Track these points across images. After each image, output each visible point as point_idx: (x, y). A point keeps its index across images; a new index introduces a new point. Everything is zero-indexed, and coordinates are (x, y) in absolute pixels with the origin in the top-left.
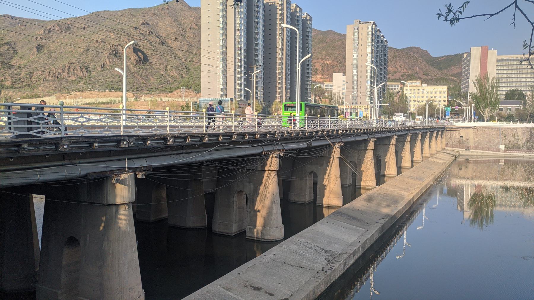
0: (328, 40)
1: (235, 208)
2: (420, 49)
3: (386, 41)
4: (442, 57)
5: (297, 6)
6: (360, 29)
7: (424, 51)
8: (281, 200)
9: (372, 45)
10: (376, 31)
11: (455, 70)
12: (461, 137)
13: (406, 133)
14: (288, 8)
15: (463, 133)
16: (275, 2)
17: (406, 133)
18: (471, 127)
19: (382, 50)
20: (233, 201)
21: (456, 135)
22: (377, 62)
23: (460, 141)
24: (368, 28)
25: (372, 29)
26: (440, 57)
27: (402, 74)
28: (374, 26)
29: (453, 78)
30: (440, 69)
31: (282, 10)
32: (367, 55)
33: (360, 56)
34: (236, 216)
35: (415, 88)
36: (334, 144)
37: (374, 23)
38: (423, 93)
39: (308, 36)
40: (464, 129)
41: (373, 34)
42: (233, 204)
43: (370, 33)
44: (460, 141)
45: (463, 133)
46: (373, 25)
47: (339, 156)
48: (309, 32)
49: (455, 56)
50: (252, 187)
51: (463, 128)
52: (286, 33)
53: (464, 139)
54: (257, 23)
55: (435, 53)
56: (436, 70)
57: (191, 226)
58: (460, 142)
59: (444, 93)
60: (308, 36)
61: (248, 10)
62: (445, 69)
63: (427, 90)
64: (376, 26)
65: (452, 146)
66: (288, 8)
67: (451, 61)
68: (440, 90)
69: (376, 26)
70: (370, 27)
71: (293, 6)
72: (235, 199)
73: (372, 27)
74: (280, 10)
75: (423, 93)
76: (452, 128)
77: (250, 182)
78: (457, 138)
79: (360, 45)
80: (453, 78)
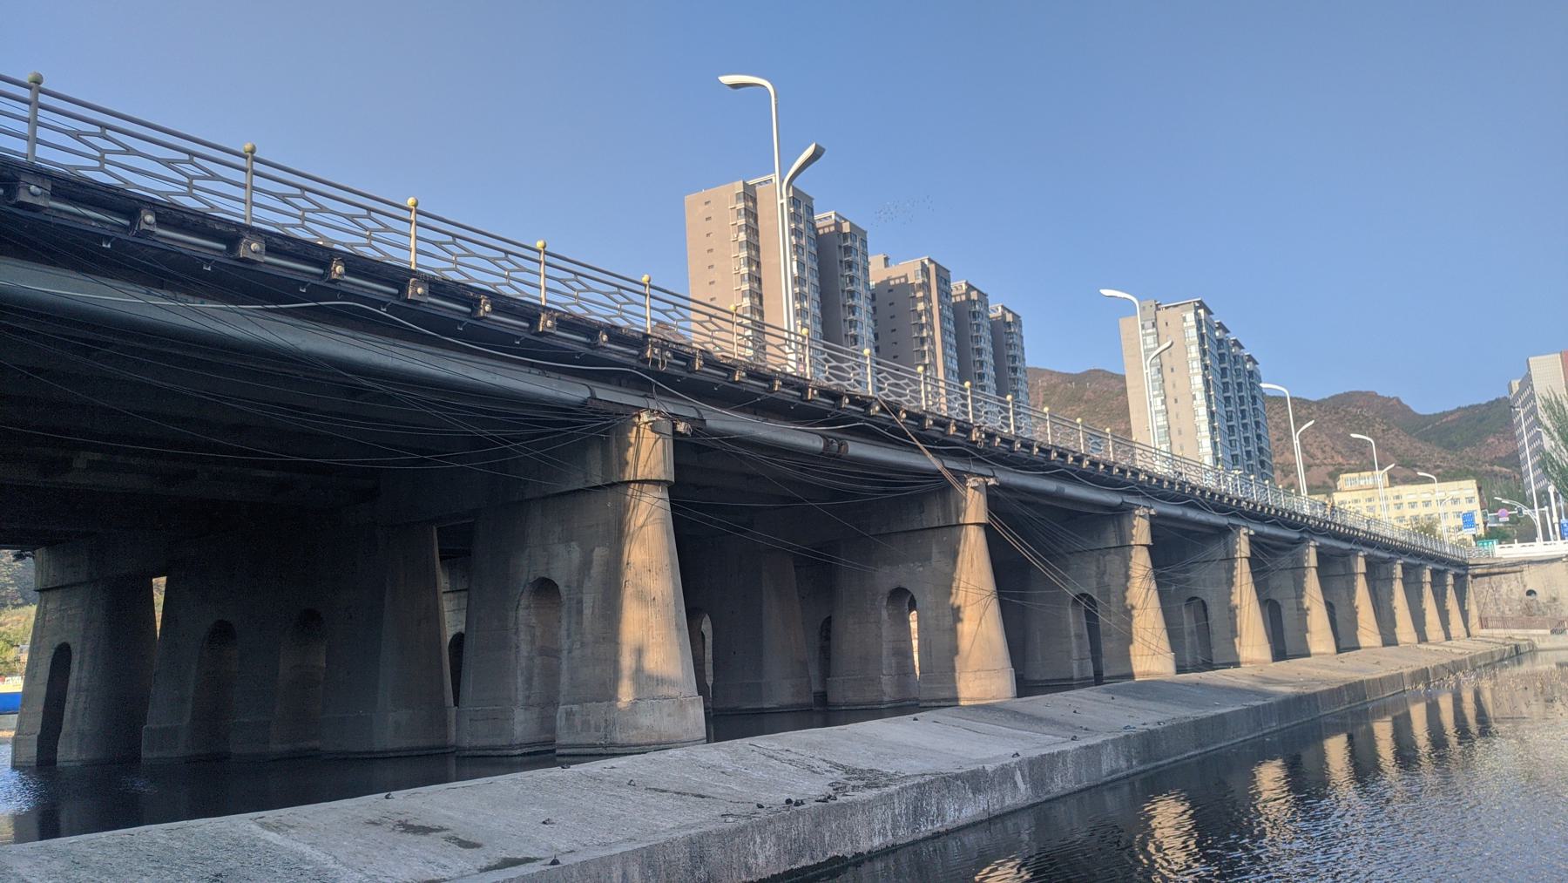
0: (1088, 395)
1: (524, 649)
2: (1374, 395)
3: (1250, 358)
4: (1452, 413)
5: (970, 288)
6: (1161, 323)
7: (1390, 399)
8: (826, 724)
9: (1206, 367)
10: (1211, 328)
11: (1495, 444)
12: (1530, 593)
13: (1294, 535)
14: (945, 293)
15: (1532, 578)
16: (906, 277)
17: (1294, 535)
18: (1559, 559)
19: (1240, 384)
20: (516, 623)
21: (1510, 587)
22: (1229, 419)
23: (1529, 607)
24: (1184, 319)
25: (1199, 322)
26: (1444, 414)
27: (1331, 468)
28: (1201, 311)
29: (1496, 468)
30: (1451, 446)
31: (927, 299)
32: (1194, 398)
33: (1170, 401)
34: (529, 681)
35: (1369, 494)
36: (960, 476)
37: (1202, 305)
38: (1399, 506)
39: (1015, 370)
40: (1533, 567)
41: (1201, 337)
42: (517, 632)
43: (1193, 333)
44: (1529, 607)
45: (1532, 578)
46: (1197, 308)
47: (983, 519)
48: (1014, 357)
49: (1490, 405)
50: (576, 555)
51: (1531, 562)
52: (945, 362)
53: (1542, 596)
54: (855, 339)
55: (1425, 404)
56: (1438, 449)
57: (390, 746)
58: (1528, 611)
59: (1470, 500)
60: (1015, 370)
61: (823, 308)
62: (1467, 445)
63: (1412, 498)
64: (1208, 312)
65: (1504, 622)
66: (945, 293)
67: (1481, 421)
68: (1455, 494)
69: (1208, 312)
70: (1190, 317)
71: (958, 287)
72: (522, 613)
73: (1196, 314)
74: (922, 299)
75: (1399, 506)
76: (1492, 566)
77: (567, 541)
78: (1516, 596)
79: (1166, 370)
80: (1496, 468)
